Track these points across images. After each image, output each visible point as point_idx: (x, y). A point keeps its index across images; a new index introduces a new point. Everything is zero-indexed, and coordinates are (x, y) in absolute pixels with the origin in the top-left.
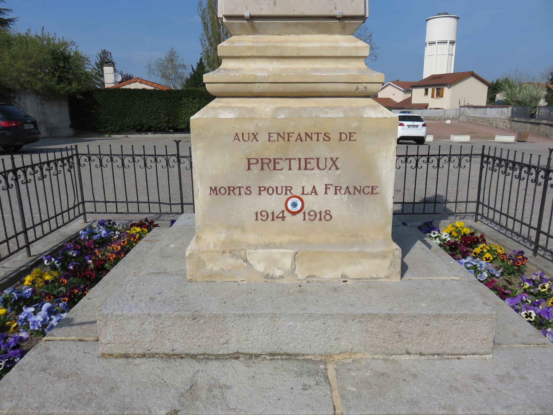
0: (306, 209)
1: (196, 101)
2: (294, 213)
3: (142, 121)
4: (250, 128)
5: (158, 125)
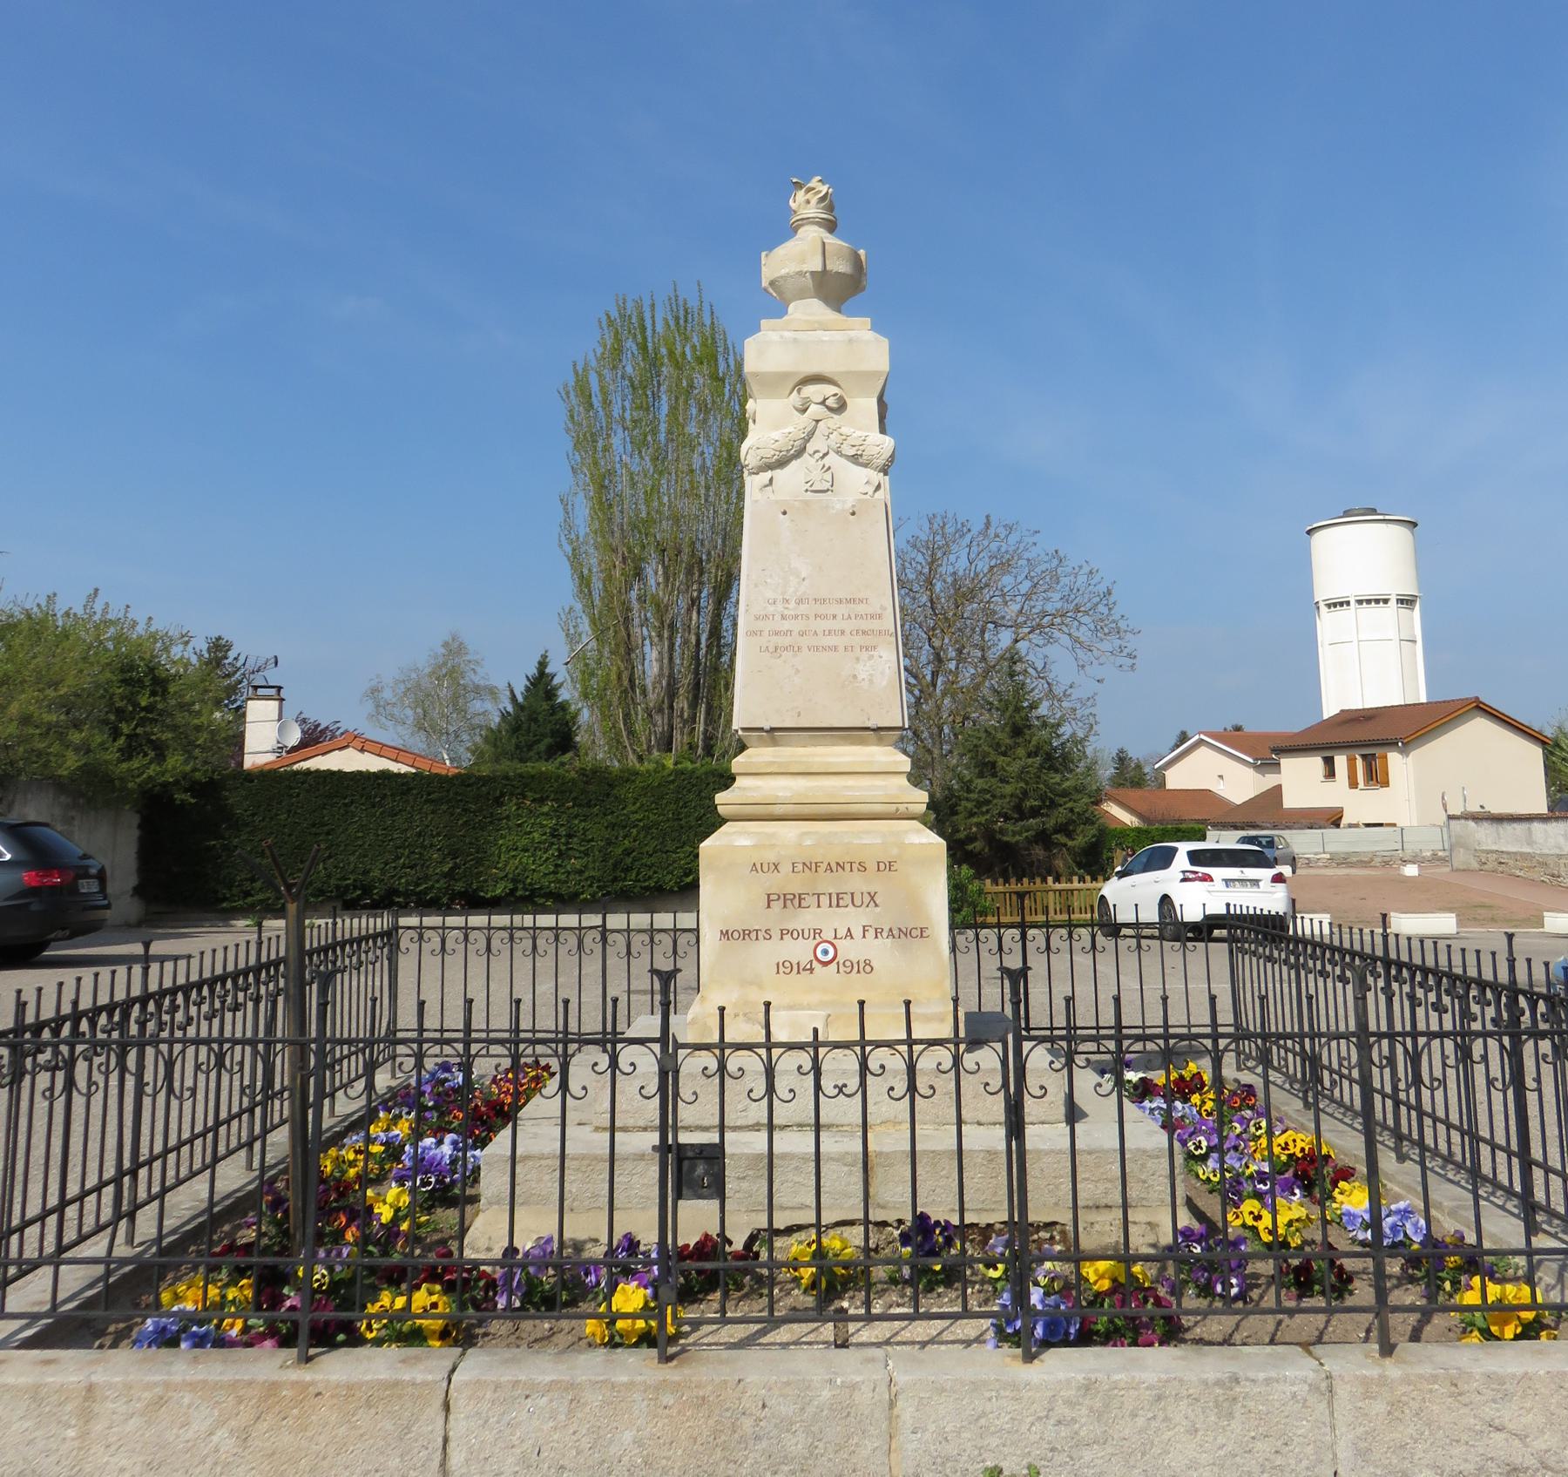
0: (840, 959)
1: (546, 809)
2: (825, 964)
3: (366, 872)
4: (771, 857)
5: (418, 885)
